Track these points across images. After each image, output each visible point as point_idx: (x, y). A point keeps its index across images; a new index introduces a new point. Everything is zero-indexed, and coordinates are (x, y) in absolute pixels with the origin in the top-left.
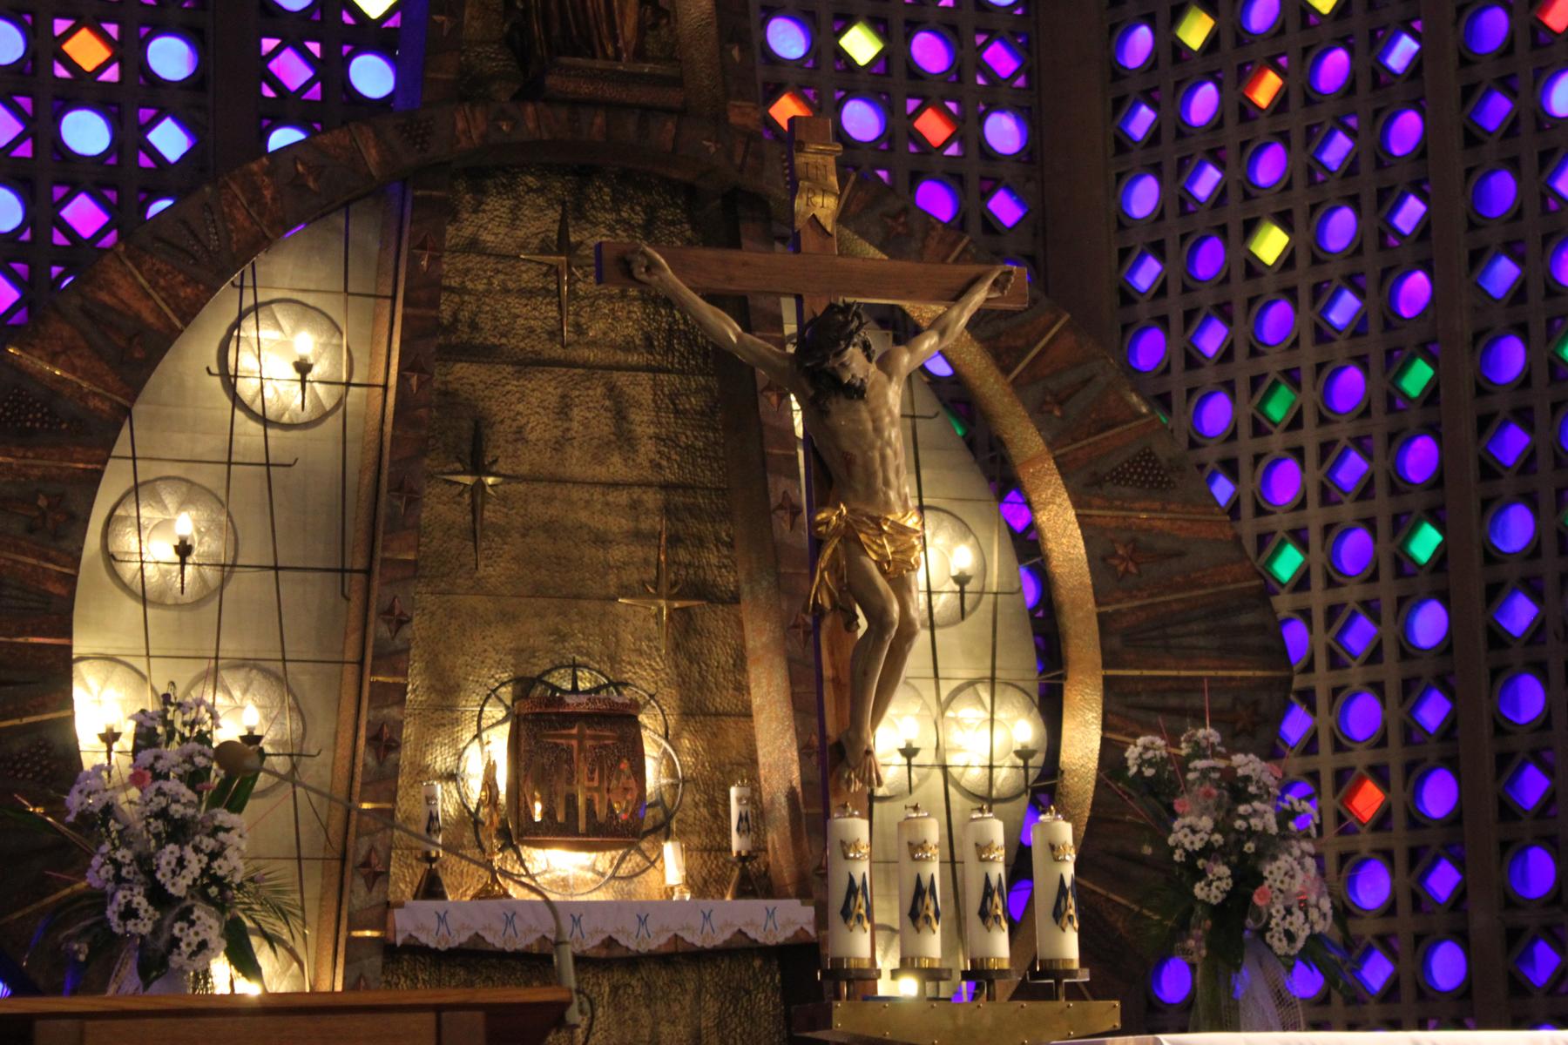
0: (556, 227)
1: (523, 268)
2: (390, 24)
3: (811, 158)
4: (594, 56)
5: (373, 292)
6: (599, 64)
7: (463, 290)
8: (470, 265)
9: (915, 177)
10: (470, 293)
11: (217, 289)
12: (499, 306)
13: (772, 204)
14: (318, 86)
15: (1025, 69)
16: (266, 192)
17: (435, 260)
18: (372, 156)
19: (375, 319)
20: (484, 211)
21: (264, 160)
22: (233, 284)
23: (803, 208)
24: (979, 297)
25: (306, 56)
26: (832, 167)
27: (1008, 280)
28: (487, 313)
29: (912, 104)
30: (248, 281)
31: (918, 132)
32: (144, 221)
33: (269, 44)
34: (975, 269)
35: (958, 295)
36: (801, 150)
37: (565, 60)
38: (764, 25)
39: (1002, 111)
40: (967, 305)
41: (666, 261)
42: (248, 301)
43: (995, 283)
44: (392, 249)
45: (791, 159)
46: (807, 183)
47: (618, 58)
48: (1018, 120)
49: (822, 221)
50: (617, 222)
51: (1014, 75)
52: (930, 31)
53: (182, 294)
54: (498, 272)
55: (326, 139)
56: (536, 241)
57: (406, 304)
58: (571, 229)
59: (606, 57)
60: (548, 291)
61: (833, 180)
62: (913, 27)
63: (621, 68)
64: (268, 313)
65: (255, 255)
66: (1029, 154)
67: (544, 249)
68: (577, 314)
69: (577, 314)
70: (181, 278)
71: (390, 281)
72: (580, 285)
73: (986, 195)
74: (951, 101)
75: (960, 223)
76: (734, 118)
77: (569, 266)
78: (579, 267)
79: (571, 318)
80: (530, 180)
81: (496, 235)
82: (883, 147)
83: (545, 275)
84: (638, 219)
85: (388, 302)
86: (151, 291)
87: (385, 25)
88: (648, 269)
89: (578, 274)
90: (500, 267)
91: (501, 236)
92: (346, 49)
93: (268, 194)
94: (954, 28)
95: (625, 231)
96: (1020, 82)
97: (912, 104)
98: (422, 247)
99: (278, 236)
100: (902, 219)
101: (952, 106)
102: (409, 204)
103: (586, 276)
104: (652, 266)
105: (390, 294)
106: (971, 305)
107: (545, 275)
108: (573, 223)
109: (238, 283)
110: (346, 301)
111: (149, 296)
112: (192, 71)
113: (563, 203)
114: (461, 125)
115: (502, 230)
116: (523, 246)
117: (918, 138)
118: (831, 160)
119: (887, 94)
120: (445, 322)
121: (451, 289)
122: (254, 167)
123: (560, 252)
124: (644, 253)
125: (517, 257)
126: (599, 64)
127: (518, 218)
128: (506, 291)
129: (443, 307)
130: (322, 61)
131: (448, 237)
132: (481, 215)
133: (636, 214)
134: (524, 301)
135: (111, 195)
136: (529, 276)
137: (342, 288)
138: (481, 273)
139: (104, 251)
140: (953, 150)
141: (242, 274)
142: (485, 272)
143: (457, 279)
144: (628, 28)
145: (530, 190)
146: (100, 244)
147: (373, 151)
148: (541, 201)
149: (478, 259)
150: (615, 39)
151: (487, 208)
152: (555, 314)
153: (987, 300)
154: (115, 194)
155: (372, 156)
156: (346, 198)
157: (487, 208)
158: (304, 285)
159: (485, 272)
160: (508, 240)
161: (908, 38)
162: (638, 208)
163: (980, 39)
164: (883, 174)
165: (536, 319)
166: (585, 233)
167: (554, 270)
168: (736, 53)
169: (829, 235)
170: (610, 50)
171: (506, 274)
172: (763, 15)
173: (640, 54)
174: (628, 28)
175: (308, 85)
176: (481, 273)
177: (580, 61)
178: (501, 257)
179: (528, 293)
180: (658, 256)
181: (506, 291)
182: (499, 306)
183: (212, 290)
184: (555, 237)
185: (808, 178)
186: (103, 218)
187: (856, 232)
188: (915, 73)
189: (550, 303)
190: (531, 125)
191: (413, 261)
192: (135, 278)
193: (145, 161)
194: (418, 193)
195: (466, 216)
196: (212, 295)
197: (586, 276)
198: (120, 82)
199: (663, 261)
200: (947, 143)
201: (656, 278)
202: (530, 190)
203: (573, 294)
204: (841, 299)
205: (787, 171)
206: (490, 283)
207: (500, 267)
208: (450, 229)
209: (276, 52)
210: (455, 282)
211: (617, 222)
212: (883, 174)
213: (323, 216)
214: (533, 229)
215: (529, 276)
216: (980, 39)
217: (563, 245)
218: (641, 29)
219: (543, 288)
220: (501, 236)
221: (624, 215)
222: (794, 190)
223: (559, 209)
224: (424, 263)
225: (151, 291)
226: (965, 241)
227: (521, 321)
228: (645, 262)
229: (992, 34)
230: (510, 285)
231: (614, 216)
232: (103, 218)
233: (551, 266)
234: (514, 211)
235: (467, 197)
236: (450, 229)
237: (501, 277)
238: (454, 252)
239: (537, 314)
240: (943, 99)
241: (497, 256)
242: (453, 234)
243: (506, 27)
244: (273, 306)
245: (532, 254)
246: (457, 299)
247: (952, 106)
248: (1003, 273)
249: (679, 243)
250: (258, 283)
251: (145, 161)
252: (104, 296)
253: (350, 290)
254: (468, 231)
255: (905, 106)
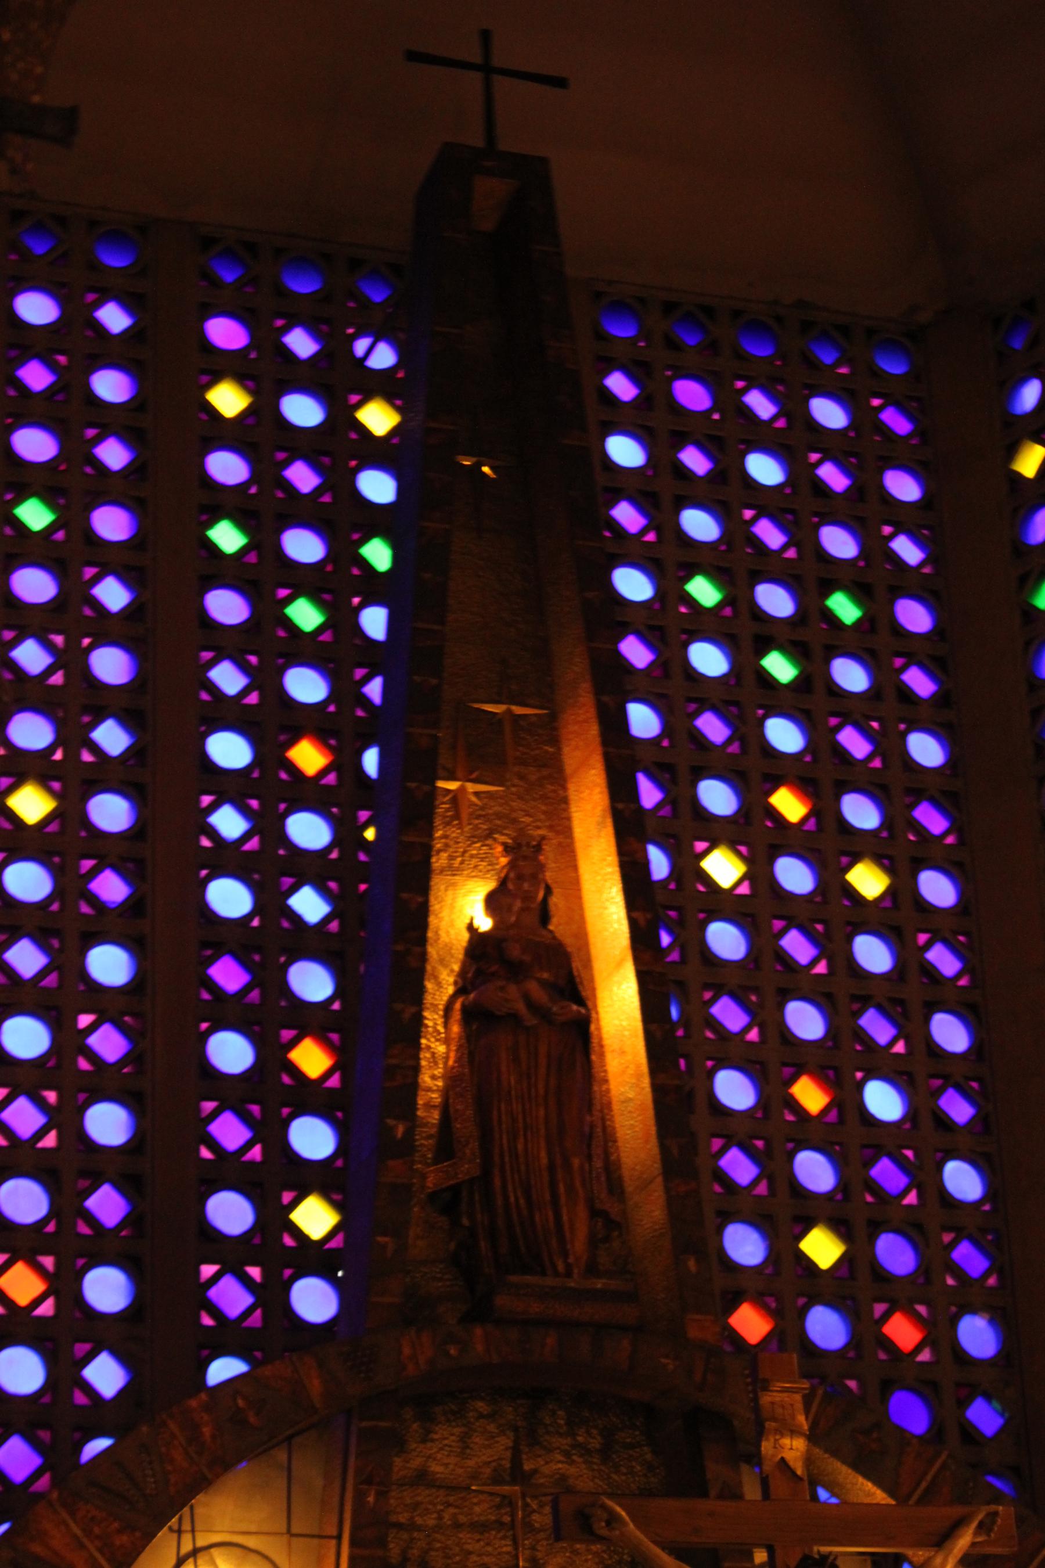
0: (509, 1454)
1: (475, 1500)
2: (332, 1244)
3: (778, 1397)
4: (544, 1273)
5: (316, 1532)
6: (549, 1281)
7: (412, 1527)
8: (419, 1499)
9: (887, 1386)
10: (419, 1529)
11: (155, 1536)
12: (449, 1542)
13: (736, 1423)
14: (258, 1312)
15: (996, 1267)
16: (205, 1430)
17: (382, 1494)
18: (315, 1386)
19: (320, 1559)
20: (433, 1440)
21: (203, 1396)
22: (171, 1529)
23: (771, 1452)
24: (964, 1541)
25: (246, 1282)
26: (799, 1406)
27: (994, 1522)
28: (437, 1550)
29: (879, 1308)
30: (186, 1526)
31: (874, 1180)
32: (77, 1465)
33: (208, 1270)
34: (957, 1511)
35: (942, 1540)
36: (766, 1389)
37: (513, 1279)
38: (720, 1231)
39: (974, 1311)
40: (951, 1551)
41: (628, 1513)
42: (187, 1547)
43: (981, 1525)
44: (337, 1485)
45: (756, 1399)
46: (773, 1424)
47: (569, 1274)
48: (992, 1322)
49: (791, 1464)
50: (573, 1446)
51: (986, 1274)
52: (897, 1231)
53: (118, 1543)
54: (449, 1505)
55: (267, 1371)
56: (488, 1471)
57: (353, 1543)
58: (524, 1457)
59: (557, 1274)
60: (502, 1524)
61: (801, 1419)
62: (876, 1227)
63: (573, 1285)
64: (207, 1558)
65: (193, 1498)
66: (1005, 1357)
67: (497, 1479)
68: (533, 1548)
69: (533, 1548)
70: (116, 1525)
71: (335, 1520)
72: (535, 1517)
73: (963, 1403)
74: (920, 1303)
75: (936, 1434)
76: (693, 1333)
77: (524, 1496)
78: (534, 1497)
79: (527, 1552)
80: (481, 1406)
81: (446, 1465)
82: (851, 1354)
83: (499, 1507)
84: (596, 1443)
85: (334, 1542)
86: (85, 1541)
87: (327, 1246)
88: (608, 1523)
89: (534, 1505)
90: (451, 1499)
91: (451, 1467)
92: (288, 1272)
93: (207, 1431)
94: (919, 1227)
95: (581, 1456)
96: (992, 1281)
97: (879, 1308)
98: (369, 1482)
99: (217, 1476)
100: (875, 1435)
101: (922, 1309)
102: (353, 1440)
103: (541, 1506)
104: (612, 1519)
105: (335, 1533)
106: (955, 1551)
107: (499, 1507)
108: (527, 1450)
109: (176, 1527)
110: (289, 1544)
111: (82, 1546)
112: (132, 677)
113: (516, 1429)
114: (407, 1351)
115: (453, 1460)
116: (474, 1477)
117: (887, 1344)
118: (798, 1397)
119: (840, 1144)
120: (393, 1561)
121: (399, 1526)
122: (193, 1403)
123: (514, 1481)
124: (604, 1507)
125: (467, 1488)
126: (549, 1281)
127: (468, 1447)
128: (457, 1526)
129: (392, 1546)
130: (262, 1286)
131: (396, 1469)
132: (429, 1444)
133: (594, 1438)
134: (477, 1536)
135: (44, 1435)
136: (481, 1509)
137: (284, 1530)
138: (430, 1507)
139: (40, 1496)
140: (925, 1356)
141: (180, 1520)
142: (435, 1505)
143: (406, 1515)
144: (579, 1244)
145: (481, 1416)
146: (33, 1488)
147: (316, 1382)
148: (492, 1428)
149: (427, 1492)
150: (566, 1256)
151: (436, 1437)
152: (509, 1549)
153: (973, 1544)
154: (48, 1434)
155: (315, 1386)
156: (288, 1433)
157: (436, 1437)
158: (244, 1527)
159: (435, 1505)
160: (460, 1471)
161: (872, 1239)
162: (594, 1432)
163: (947, 1238)
164: (852, 1384)
165: (489, 1554)
166: (539, 1459)
167: (508, 1501)
168: (692, 1264)
169: (800, 1479)
170: (561, 1267)
171: (457, 1507)
172: (719, 1220)
173: (592, 1269)
174: (579, 1244)
175: (248, 1312)
176: (430, 1507)
177: (529, 1279)
178: (452, 1488)
179: (481, 1527)
180: (618, 1509)
181: (457, 1526)
182: (449, 1542)
183: (149, 1536)
184: (508, 1465)
185: (774, 1419)
186: (36, 1461)
187: (826, 1451)
188: (880, 1275)
189: (504, 1538)
190: (480, 1348)
191: (359, 1498)
192: (67, 1526)
193: (80, 1398)
194: (364, 1424)
195: (414, 1446)
196: (150, 1541)
197: (541, 1506)
198: (56, 1316)
199: (623, 1513)
200: (918, 1348)
201: (617, 1532)
202: (481, 1416)
203: (529, 1528)
204: (815, 1549)
205: (750, 1388)
206: (440, 1518)
207: (451, 1499)
208: (398, 1461)
209: (215, 1279)
210: (403, 1518)
211: (573, 1446)
212: (852, 1384)
213: (265, 1451)
214: (484, 1458)
215: (481, 1509)
216: (947, 1238)
217: (517, 1474)
218: (593, 1242)
219: (496, 1521)
220: (451, 1467)
221: (580, 1439)
222: (760, 1432)
223: (511, 1434)
224: (371, 1499)
225: (85, 1541)
226: (944, 1457)
227: (474, 1558)
228: (605, 1516)
229: (961, 1233)
230: (462, 1519)
231: (569, 1440)
232: (36, 1461)
233: (504, 1497)
234: (464, 1440)
235: (415, 1426)
236: (398, 1461)
237: (452, 1510)
238: (402, 1485)
239: (490, 1549)
240: (912, 1301)
241: (448, 1488)
242: (401, 1466)
243: (452, 1246)
244: (212, 1550)
245: (484, 1485)
246: (405, 1536)
247: (922, 1309)
248: (988, 1515)
249: (639, 1468)
250: (198, 1527)
251: (80, 1398)
252: (37, 1548)
253: (294, 1530)
254: (416, 1463)
255: (871, 1310)
